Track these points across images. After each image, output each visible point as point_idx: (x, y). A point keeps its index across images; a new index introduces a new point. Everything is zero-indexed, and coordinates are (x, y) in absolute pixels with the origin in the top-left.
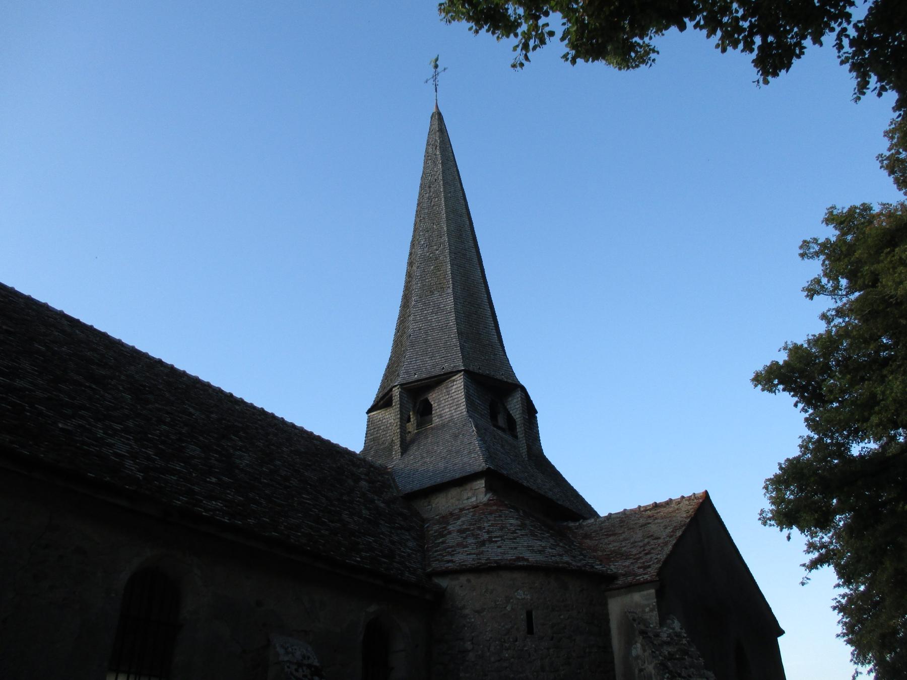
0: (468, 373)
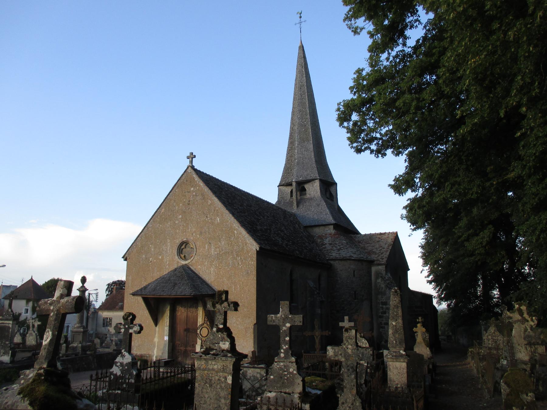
0: (321, 181)
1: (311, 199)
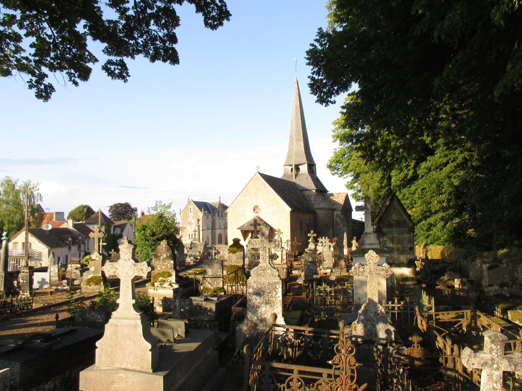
0: (308, 164)
1: (302, 174)
